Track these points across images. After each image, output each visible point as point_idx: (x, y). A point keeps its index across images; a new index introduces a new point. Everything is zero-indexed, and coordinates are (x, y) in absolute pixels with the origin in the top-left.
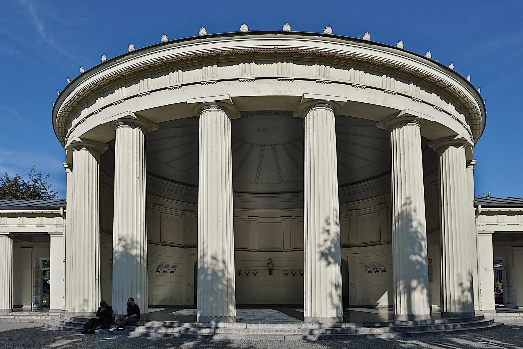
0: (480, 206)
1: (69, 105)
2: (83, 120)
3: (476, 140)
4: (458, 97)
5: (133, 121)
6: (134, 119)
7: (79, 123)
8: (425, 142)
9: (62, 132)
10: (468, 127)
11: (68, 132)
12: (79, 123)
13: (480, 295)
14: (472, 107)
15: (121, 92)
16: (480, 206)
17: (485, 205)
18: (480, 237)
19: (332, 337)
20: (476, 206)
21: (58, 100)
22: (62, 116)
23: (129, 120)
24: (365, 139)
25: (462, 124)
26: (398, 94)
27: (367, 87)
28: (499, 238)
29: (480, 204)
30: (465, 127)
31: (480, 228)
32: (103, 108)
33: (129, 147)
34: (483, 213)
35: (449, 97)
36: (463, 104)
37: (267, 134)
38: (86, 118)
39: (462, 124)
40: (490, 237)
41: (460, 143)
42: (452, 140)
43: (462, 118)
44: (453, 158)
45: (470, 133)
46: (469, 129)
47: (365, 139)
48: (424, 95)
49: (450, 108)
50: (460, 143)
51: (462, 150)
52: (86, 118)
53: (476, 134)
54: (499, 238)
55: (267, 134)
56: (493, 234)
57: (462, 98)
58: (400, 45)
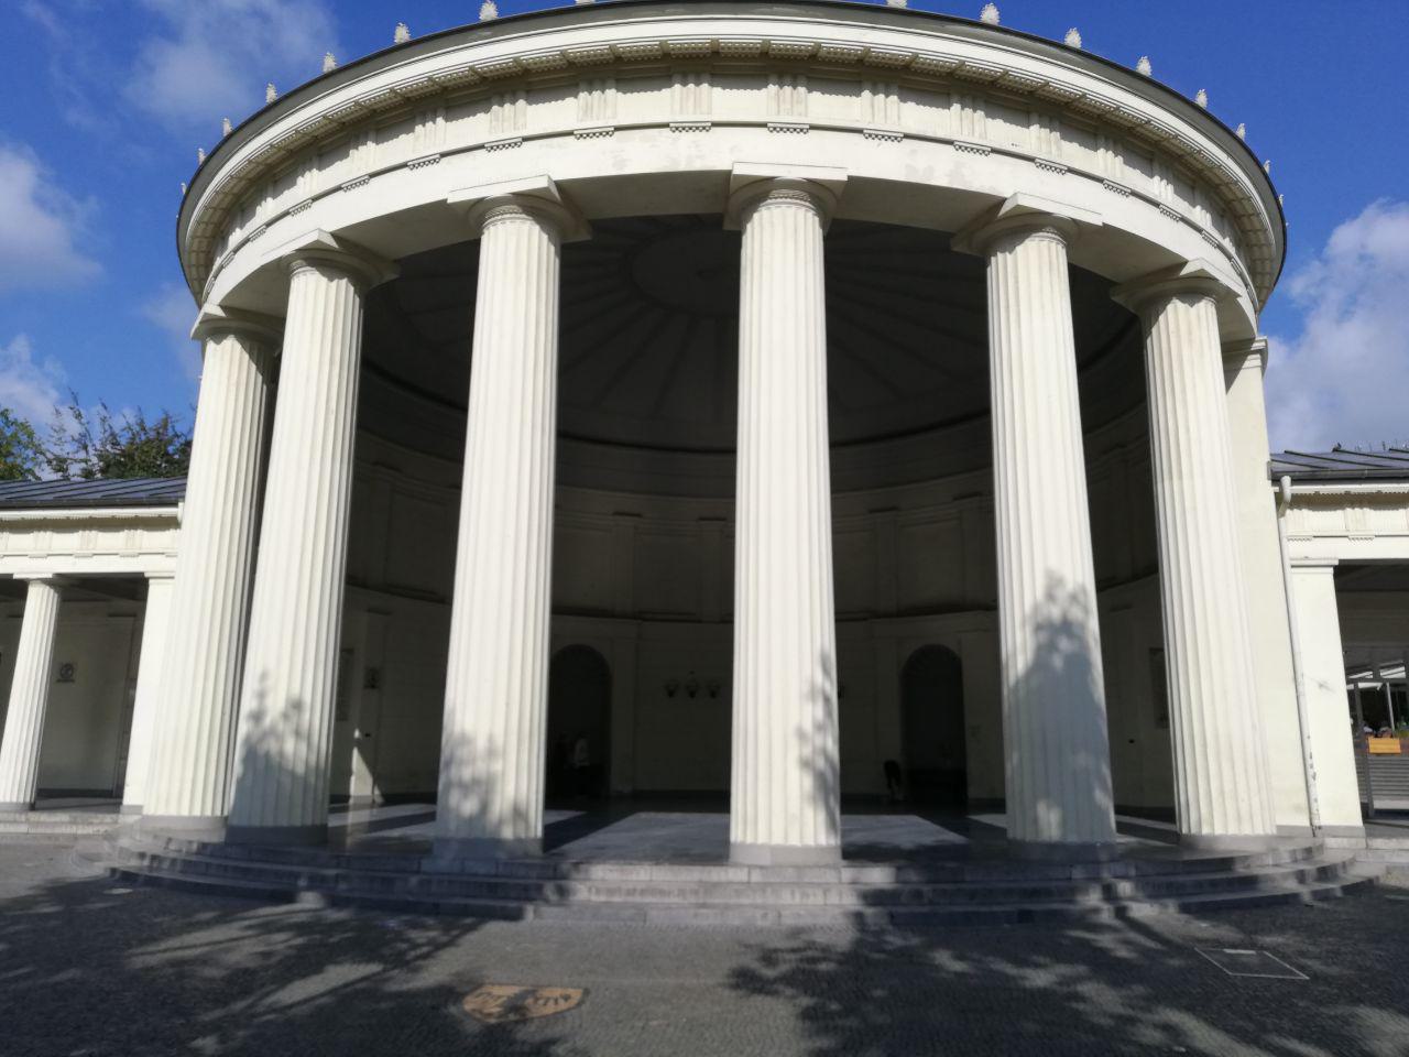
0: (1286, 480)
1: (205, 219)
2: (260, 232)
3: (1265, 291)
4: (1217, 182)
5: (329, 256)
6: (328, 249)
7: (247, 241)
8: (1081, 282)
9: (198, 266)
10: (1227, 243)
11: (215, 267)
12: (247, 241)
13: (1310, 772)
14: (1240, 196)
15: (368, 155)
16: (1286, 480)
17: (1309, 478)
18: (1298, 579)
19: (836, 989)
20: (1275, 479)
21: (186, 203)
22: (199, 234)
23: (318, 255)
24: (907, 285)
25: (1199, 230)
26: (994, 151)
27: (907, 136)
28: (1354, 580)
29: (1287, 473)
30: (1208, 238)
31: (1295, 550)
32: (315, 199)
33: (321, 320)
34: (1300, 502)
35: (1152, 153)
36: (1228, 203)
37: (648, 275)
38: (269, 224)
39: (1199, 230)
40: (1327, 580)
41: (1198, 287)
42: (1167, 280)
43: (1201, 216)
44: (1184, 340)
45: (1230, 258)
46: (1232, 250)
47: (907, 285)
48: (1074, 153)
49: (1160, 188)
50: (1198, 287)
51: (1205, 310)
52: (269, 224)
53: (1263, 274)
54: (1354, 580)
55: (648, 275)
56: (1335, 568)
57: (1227, 184)
58: (990, 15)
